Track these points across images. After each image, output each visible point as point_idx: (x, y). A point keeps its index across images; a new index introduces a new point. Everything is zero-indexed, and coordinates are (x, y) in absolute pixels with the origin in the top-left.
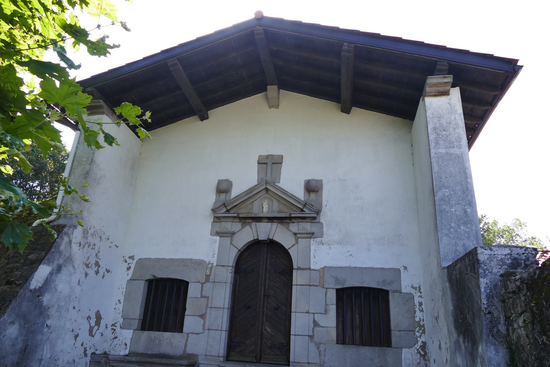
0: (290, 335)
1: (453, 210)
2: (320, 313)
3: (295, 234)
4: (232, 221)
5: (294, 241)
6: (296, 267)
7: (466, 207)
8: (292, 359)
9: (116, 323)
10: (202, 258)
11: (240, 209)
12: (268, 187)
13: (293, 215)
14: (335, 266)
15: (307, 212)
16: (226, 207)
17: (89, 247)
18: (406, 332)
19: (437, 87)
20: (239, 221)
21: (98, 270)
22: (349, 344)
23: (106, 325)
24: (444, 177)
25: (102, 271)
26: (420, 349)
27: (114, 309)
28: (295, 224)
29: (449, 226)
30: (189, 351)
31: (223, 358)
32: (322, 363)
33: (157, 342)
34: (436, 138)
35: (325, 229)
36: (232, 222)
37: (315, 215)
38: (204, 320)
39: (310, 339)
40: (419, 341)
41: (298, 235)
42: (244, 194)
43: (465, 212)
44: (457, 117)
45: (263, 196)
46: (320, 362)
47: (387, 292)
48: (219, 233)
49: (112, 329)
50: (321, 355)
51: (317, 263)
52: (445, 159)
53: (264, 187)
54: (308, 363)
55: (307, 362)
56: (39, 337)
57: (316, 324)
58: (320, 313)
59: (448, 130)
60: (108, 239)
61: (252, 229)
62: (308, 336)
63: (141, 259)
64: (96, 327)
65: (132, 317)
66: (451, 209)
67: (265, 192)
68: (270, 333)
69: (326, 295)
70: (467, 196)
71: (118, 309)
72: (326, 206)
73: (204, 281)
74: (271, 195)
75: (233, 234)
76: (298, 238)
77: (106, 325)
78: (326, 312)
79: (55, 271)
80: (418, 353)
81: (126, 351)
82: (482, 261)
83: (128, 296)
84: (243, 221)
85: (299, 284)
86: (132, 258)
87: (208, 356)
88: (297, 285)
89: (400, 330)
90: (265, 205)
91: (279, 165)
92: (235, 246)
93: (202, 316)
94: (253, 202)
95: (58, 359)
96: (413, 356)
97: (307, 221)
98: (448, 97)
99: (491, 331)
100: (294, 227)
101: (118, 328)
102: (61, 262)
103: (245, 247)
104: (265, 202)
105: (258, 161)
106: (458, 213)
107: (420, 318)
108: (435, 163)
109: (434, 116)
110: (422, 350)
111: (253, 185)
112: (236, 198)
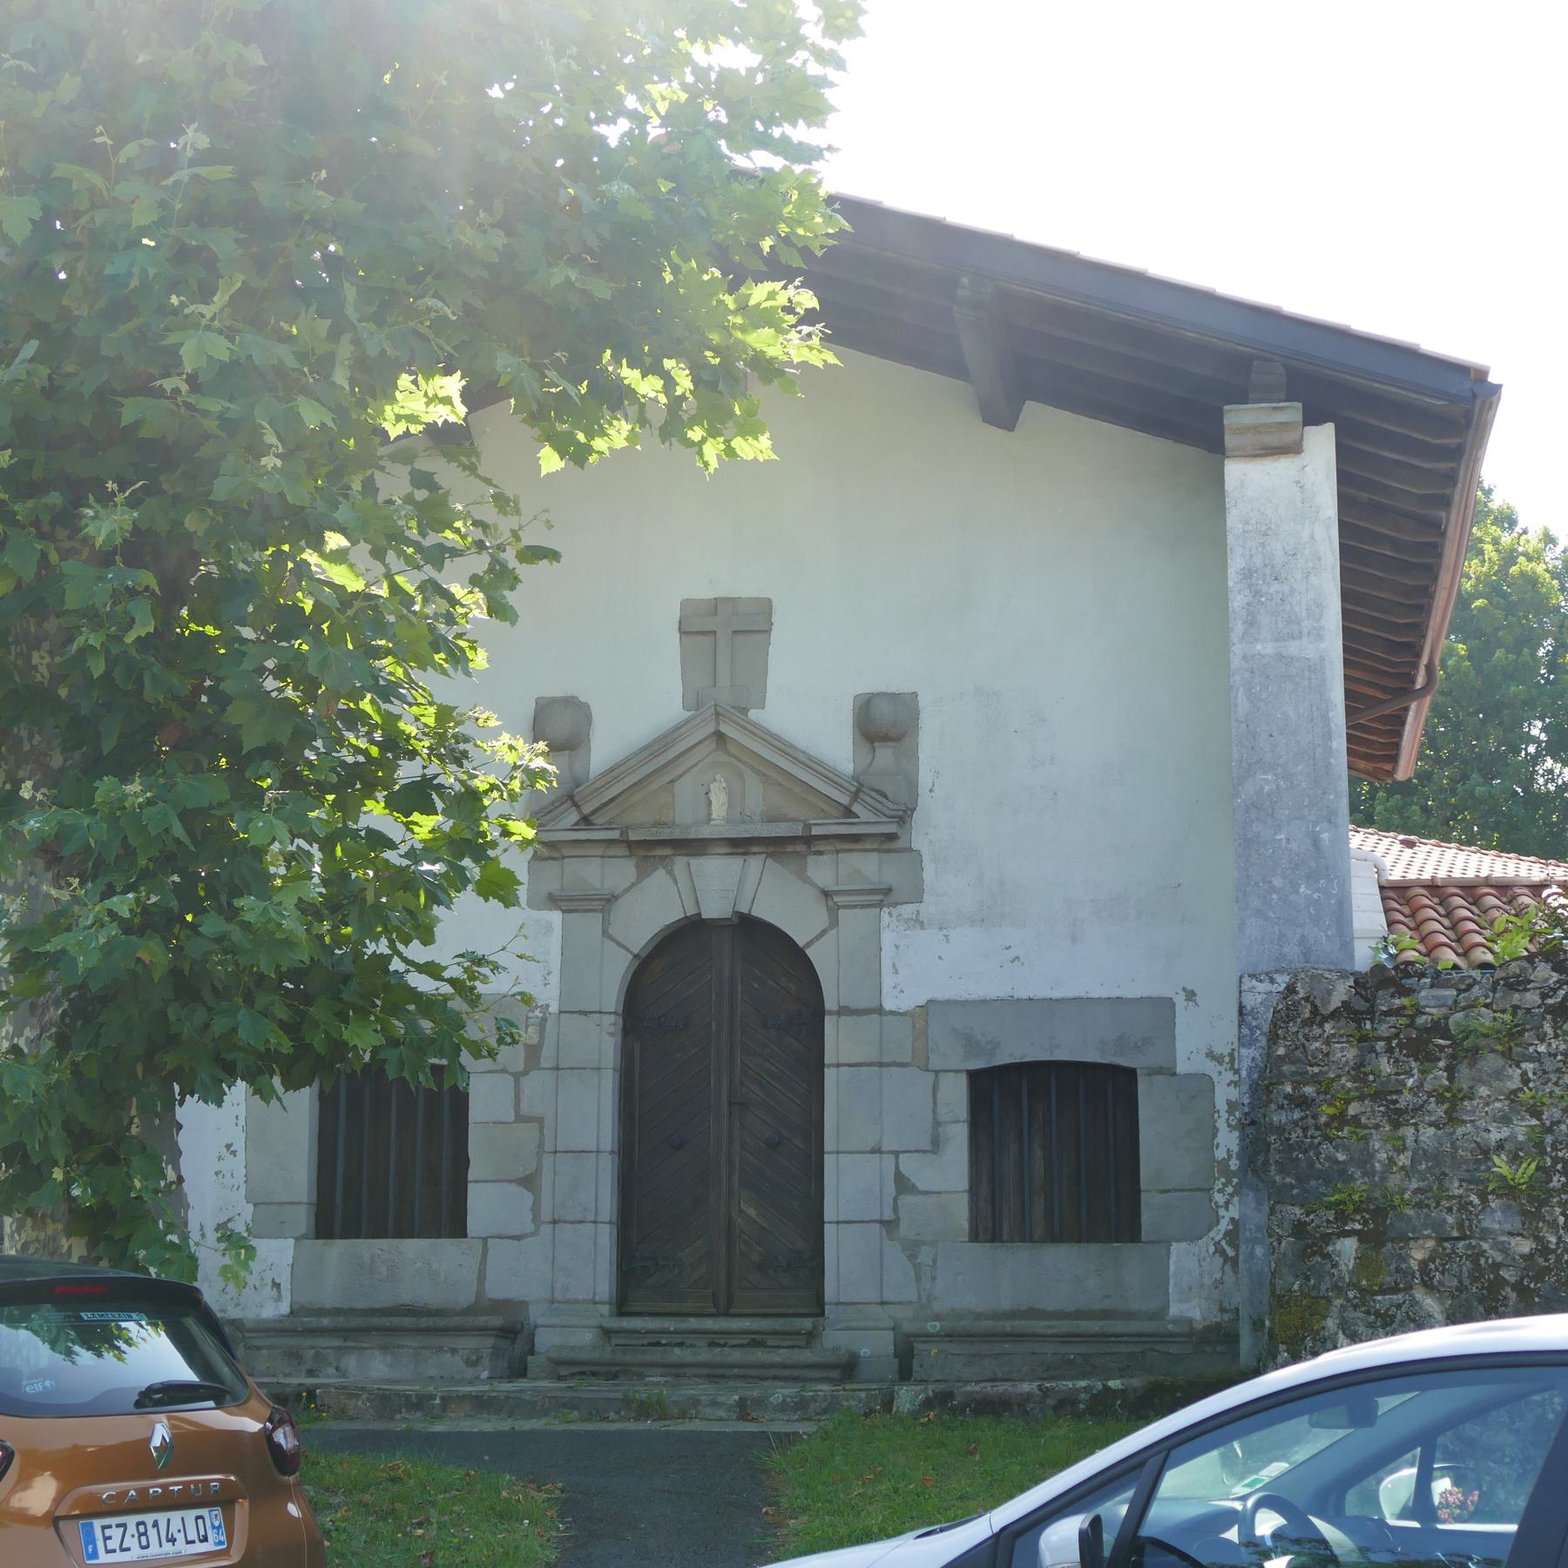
0: (823, 1223)
1: (1282, 836)
2: (917, 1151)
3: (827, 894)
4: (600, 853)
5: (821, 918)
6: (836, 1008)
7: (1318, 829)
8: (830, 1294)
9: (230, 1220)
12: (723, 728)
13: (815, 831)
14: (965, 996)
15: (867, 819)
18: (1186, 1193)
19: (1260, 432)
20: (627, 853)
22: (1012, 1240)
26: (1223, 1243)
27: (217, 1174)
28: (824, 858)
29: (1266, 887)
30: (497, 1289)
31: (608, 1306)
32: (924, 1301)
33: (384, 1270)
34: (1248, 604)
35: (928, 874)
36: (602, 857)
37: (891, 828)
38: (533, 1194)
39: (887, 1231)
40: (1223, 1217)
41: (836, 899)
43: (1316, 842)
44: (1320, 532)
45: (707, 760)
46: (920, 1298)
47: (1131, 1074)
48: (561, 900)
50: (923, 1278)
51: (898, 992)
52: (1272, 677)
53: (710, 729)
54: (882, 1303)
55: (879, 1301)
57: (903, 1184)
58: (917, 1151)
59: (1286, 579)
61: (676, 881)
62: (881, 1222)
65: (285, 1199)
66: (1276, 834)
67: (714, 746)
68: (756, 1222)
69: (934, 1094)
70: (1324, 793)
71: (228, 1175)
72: (931, 791)
73: (521, 1067)
74: (735, 756)
75: (611, 899)
76: (839, 907)
78: (936, 1145)
80: (1217, 1255)
82: (1249, 1008)
84: (481, 602)
85: (847, 1062)
87: (559, 1302)
88: (838, 1065)
89: (1167, 1188)
92: (619, 944)
93: (529, 1182)
94: (673, 781)
96: (1203, 1263)
97: (868, 846)
98: (1298, 461)
99: (1252, 1162)
100: (822, 870)
104: (715, 784)
105: (680, 622)
106: (1294, 845)
107: (1228, 1150)
108: (1241, 690)
109: (1251, 528)
110: (1230, 1244)
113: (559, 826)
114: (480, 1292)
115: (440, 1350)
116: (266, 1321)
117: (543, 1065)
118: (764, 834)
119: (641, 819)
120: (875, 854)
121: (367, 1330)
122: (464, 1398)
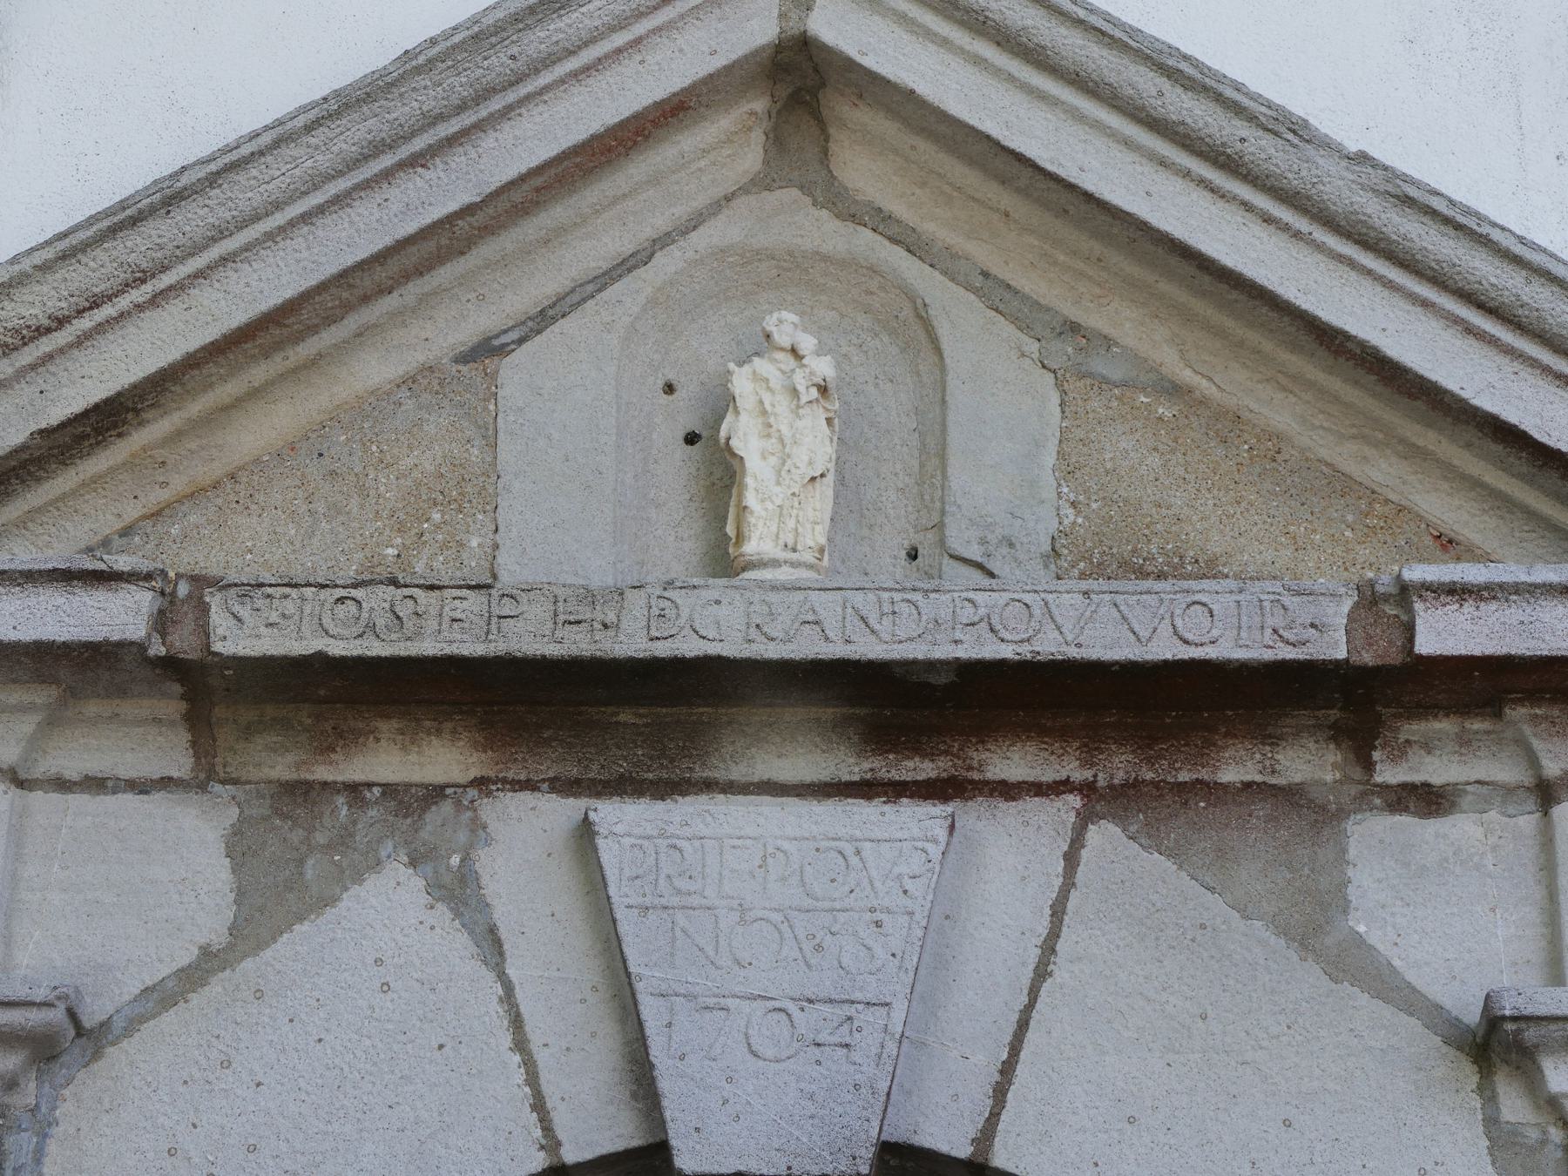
11: (194, 495)
20: (179, 763)
42: (305, 159)
61: (492, 946)
67: (751, 158)
74: (880, 221)
81: (732, 1008)
84: (282, 768)
90: (781, 405)
94: (487, 350)
111: (1151, 29)
112: (137, 246)
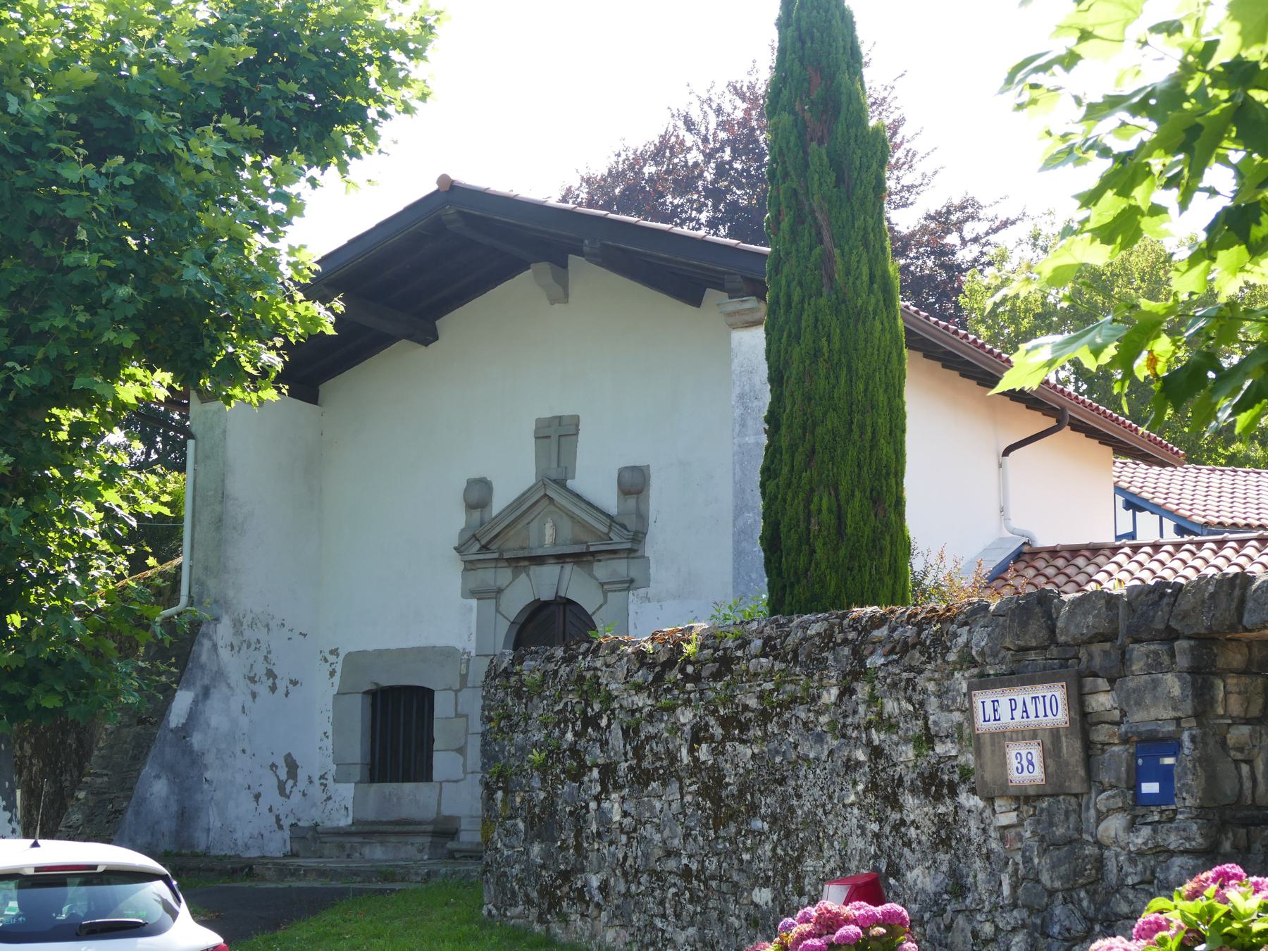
3: (602, 584)
5: (599, 599)
10: (451, 644)
13: (592, 549)
16: (477, 540)
17: (248, 647)
21: (274, 684)
23: (310, 777)
24: (749, 490)
25: (282, 685)
30: (446, 811)
33: (395, 800)
49: (321, 784)
56: (199, 797)
60: (283, 625)
63: (350, 654)
64: (290, 782)
73: (458, 687)
77: (310, 777)
79: (200, 698)
83: (338, 724)
86: (334, 652)
91: (574, 437)
95: (235, 830)
100: (602, 570)
101: (330, 782)
102: (206, 681)
103: (526, 615)
113: (471, 552)
114: (438, 812)
115: (406, 843)
116: (342, 828)
117: (469, 685)
118: (568, 552)
119: (512, 546)
120: (625, 560)
121: (373, 833)
122: (314, 870)
